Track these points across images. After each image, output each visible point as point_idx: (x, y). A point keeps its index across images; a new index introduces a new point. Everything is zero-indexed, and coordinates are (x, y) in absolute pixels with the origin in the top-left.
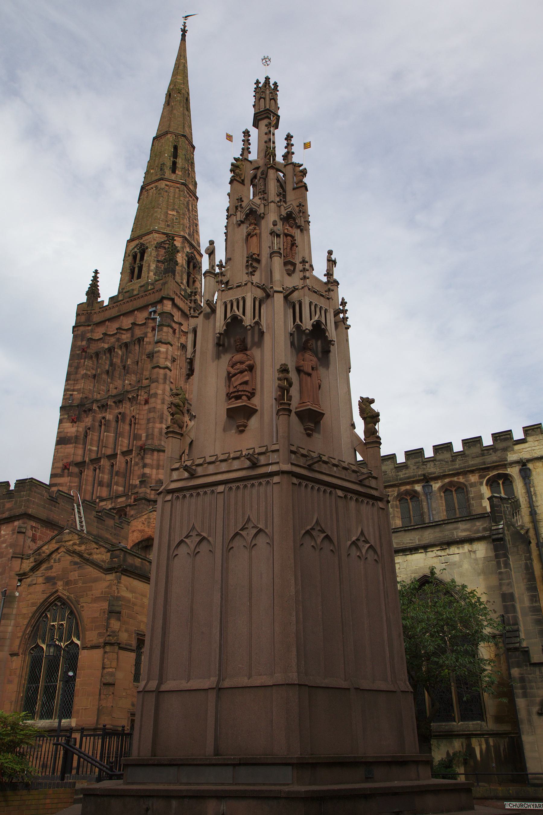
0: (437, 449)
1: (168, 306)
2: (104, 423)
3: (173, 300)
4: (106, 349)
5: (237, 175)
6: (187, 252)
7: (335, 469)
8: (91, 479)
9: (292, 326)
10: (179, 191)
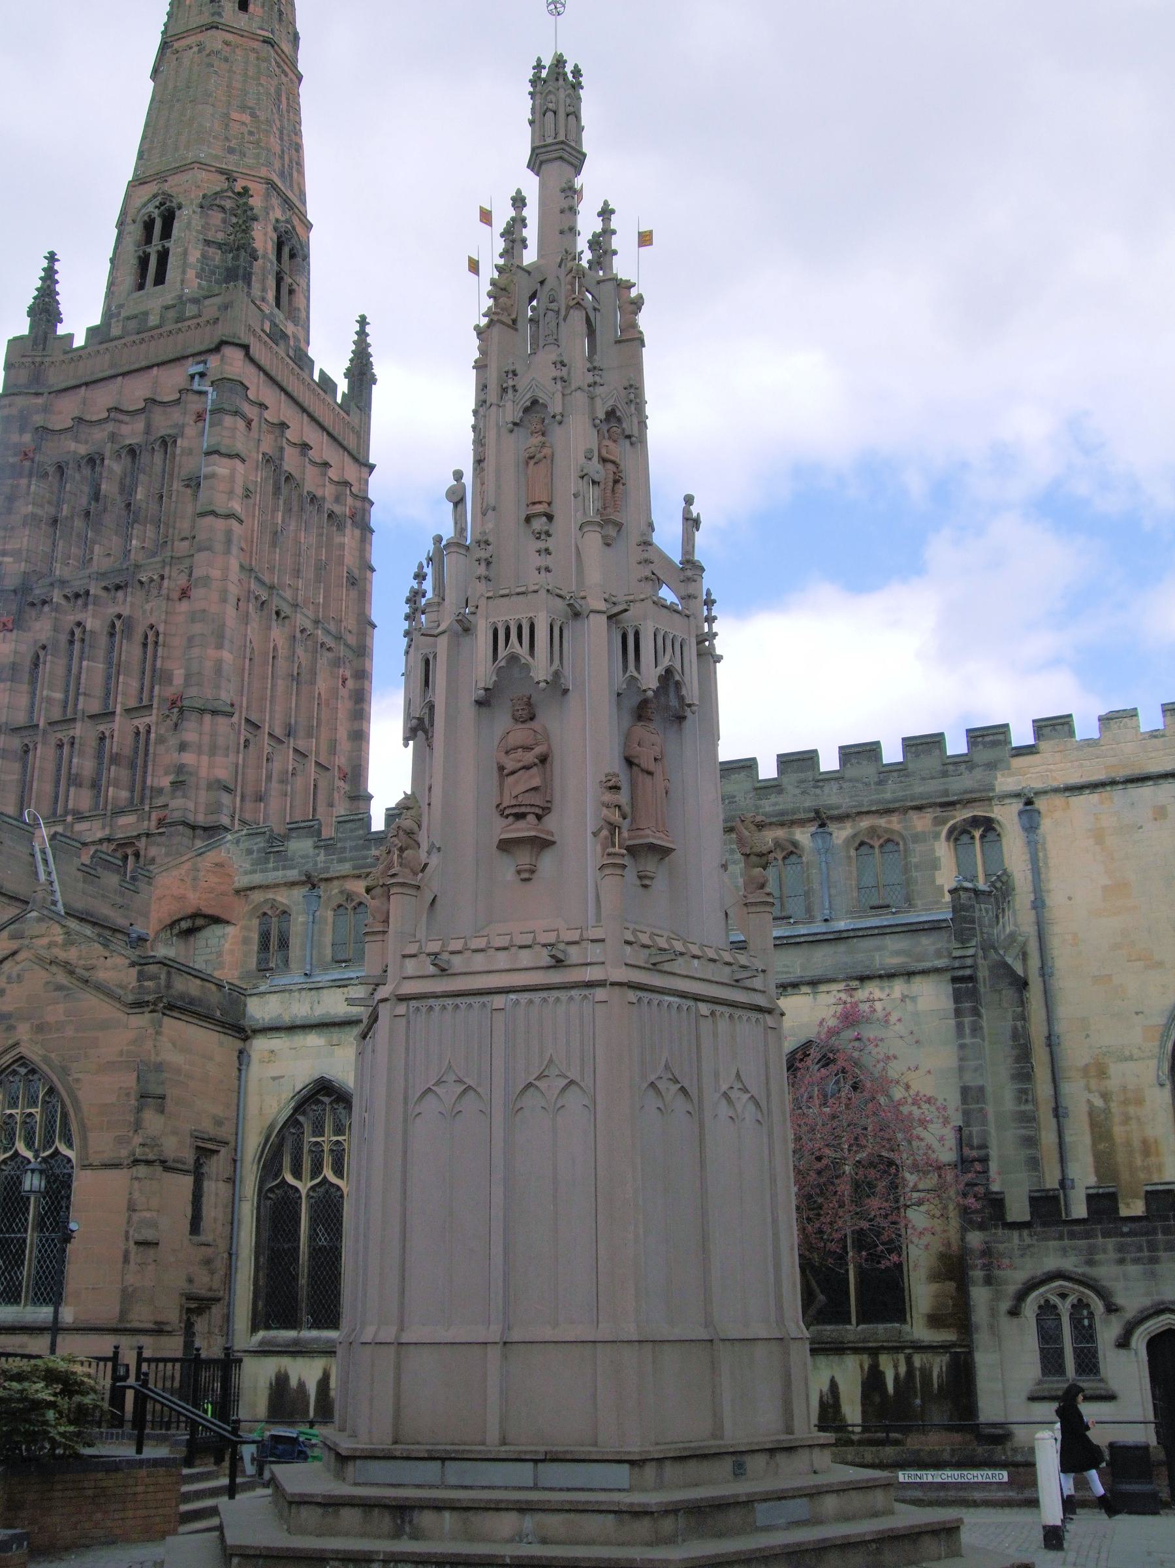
0: (848, 754)
1: (233, 363)
2: (76, 636)
3: (246, 348)
4: (82, 458)
5: (502, 309)
6: (277, 221)
7: (696, 961)
8: (51, 766)
9: (621, 679)
10: (258, 59)
